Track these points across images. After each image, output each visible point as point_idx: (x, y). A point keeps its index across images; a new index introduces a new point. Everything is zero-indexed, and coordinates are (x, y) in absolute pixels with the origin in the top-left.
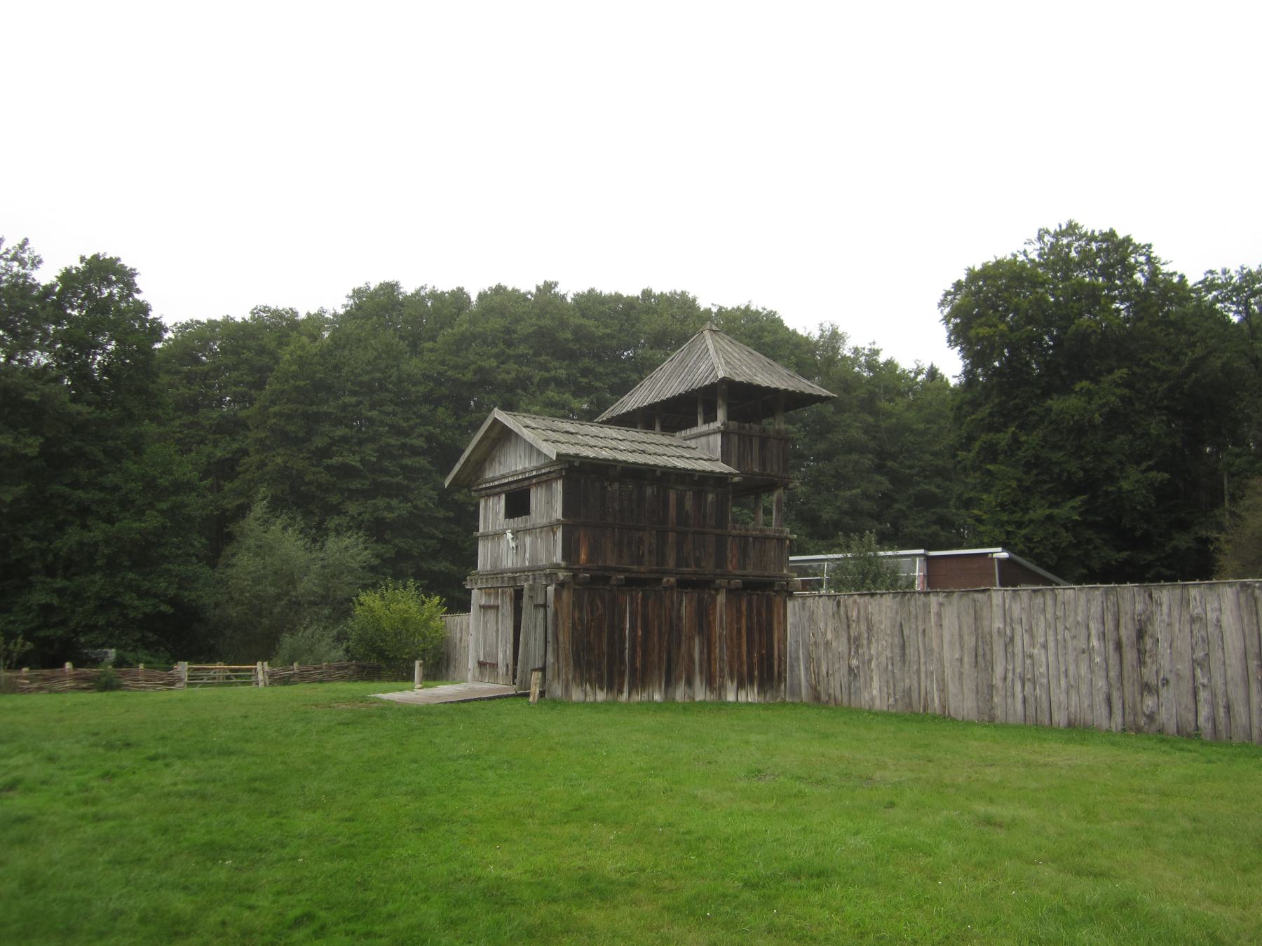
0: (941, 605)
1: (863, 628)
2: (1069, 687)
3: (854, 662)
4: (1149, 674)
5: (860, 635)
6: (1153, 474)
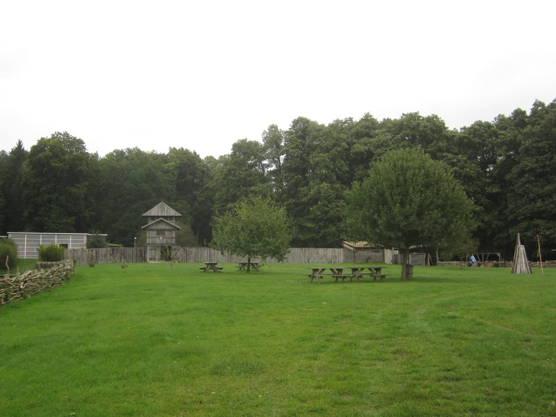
0: (204, 249)
1: (190, 253)
2: (222, 259)
3: (188, 257)
4: (232, 257)
5: (189, 254)
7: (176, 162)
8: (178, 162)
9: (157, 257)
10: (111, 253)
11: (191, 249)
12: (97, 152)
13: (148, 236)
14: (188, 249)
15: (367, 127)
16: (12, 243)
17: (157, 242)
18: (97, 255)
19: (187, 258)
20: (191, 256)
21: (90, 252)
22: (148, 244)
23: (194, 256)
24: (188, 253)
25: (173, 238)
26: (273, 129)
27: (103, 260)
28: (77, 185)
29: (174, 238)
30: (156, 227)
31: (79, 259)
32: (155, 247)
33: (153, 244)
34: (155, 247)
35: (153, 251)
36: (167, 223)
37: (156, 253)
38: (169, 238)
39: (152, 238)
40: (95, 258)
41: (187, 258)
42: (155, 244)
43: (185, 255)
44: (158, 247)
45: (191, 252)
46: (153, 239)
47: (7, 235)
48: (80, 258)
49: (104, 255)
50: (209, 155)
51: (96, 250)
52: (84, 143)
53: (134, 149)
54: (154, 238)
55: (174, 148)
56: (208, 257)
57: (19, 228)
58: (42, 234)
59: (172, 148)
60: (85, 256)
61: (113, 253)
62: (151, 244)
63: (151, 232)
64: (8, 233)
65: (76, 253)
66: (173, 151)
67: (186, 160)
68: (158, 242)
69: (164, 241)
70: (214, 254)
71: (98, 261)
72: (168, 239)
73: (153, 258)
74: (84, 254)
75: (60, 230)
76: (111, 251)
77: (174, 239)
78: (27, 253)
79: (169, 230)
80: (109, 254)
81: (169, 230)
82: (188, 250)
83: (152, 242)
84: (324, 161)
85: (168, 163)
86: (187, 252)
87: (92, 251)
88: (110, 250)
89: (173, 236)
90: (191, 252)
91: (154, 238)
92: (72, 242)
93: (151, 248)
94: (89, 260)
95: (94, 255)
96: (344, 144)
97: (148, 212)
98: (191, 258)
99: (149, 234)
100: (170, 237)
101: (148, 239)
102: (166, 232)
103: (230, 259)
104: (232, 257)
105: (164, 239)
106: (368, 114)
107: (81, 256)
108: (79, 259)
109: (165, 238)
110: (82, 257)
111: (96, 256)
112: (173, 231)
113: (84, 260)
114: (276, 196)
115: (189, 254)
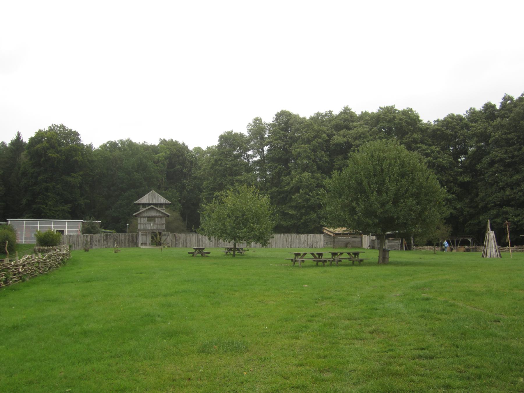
0: (192, 235)
1: (179, 238)
2: (209, 244)
3: (177, 243)
4: (219, 243)
5: (178, 239)
6: (86, 200)
7: (165, 153)
8: (168, 153)
9: (148, 242)
10: (105, 238)
11: (180, 235)
12: (91, 143)
13: (139, 222)
14: (177, 235)
15: (346, 120)
16: (11, 229)
17: (148, 228)
18: (92, 240)
19: (176, 244)
20: (180, 241)
21: (85, 237)
22: (140, 230)
23: (182, 242)
24: (177, 238)
25: (163, 224)
26: (258, 121)
27: (97, 245)
28: (73, 174)
29: (164, 224)
30: (147, 214)
31: (75, 244)
32: (146, 233)
33: (144, 230)
34: (146, 233)
35: (145, 237)
36: (157, 210)
37: (147, 238)
38: (159, 224)
39: (143, 224)
40: (89, 243)
41: (176, 244)
42: (146, 230)
43: (175, 241)
44: (149, 233)
45: (180, 238)
46: (145, 226)
47: (7, 221)
48: (76, 244)
49: (98, 241)
50: (197, 146)
51: (91, 236)
52: (79, 135)
53: (126, 140)
54: (146, 224)
55: (164, 139)
56: (196, 242)
57: (18, 214)
58: (40, 221)
59: (162, 139)
60: (80, 242)
61: (107, 239)
62: (142, 230)
63: (142, 218)
64: (7, 219)
65: (72, 238)
66: (163, 142)
67: (175, 151)
68: (149, 228)
69: (155, 227)
70: (202, 240)
71: (92, 246)
72: (158, 226)
73: (144, 244)
74: (79, 239)
75: (57, 217)
76: (105, 236)
77: (164, 225)
78: (26, 239)
79: (159, 217)
80: (103, 239)
81: (159, 217)
82: (177, 236)
83: (143, 228)
84: (305, 151)
85: (158, 153)
86: (176, 238)
87: (87, 236)
88: (104, 236)
89: (163, 223)
90: (180, 238)
91: (146, 224)
92: (68, 228)
93: (142, 234)
94: (84, 245)
95: (89, 240)
96: (324, 136)
97: (140, 200)
98: (180, 243)
99: (140, 221)
100: (160, 223)
101: (139, 225)
102: (156, 219)
103: (217, 244)
104: (219, 243)
105: (155, 225)
106: (347, 107)
107: (77, 242)
108: (75, 244)
109: (156, 224)
110: (77, 242)
111: (91, 241)
112: (163, 218)
113: (79, 245)
114: (260, 185)
115: (178, 239)
